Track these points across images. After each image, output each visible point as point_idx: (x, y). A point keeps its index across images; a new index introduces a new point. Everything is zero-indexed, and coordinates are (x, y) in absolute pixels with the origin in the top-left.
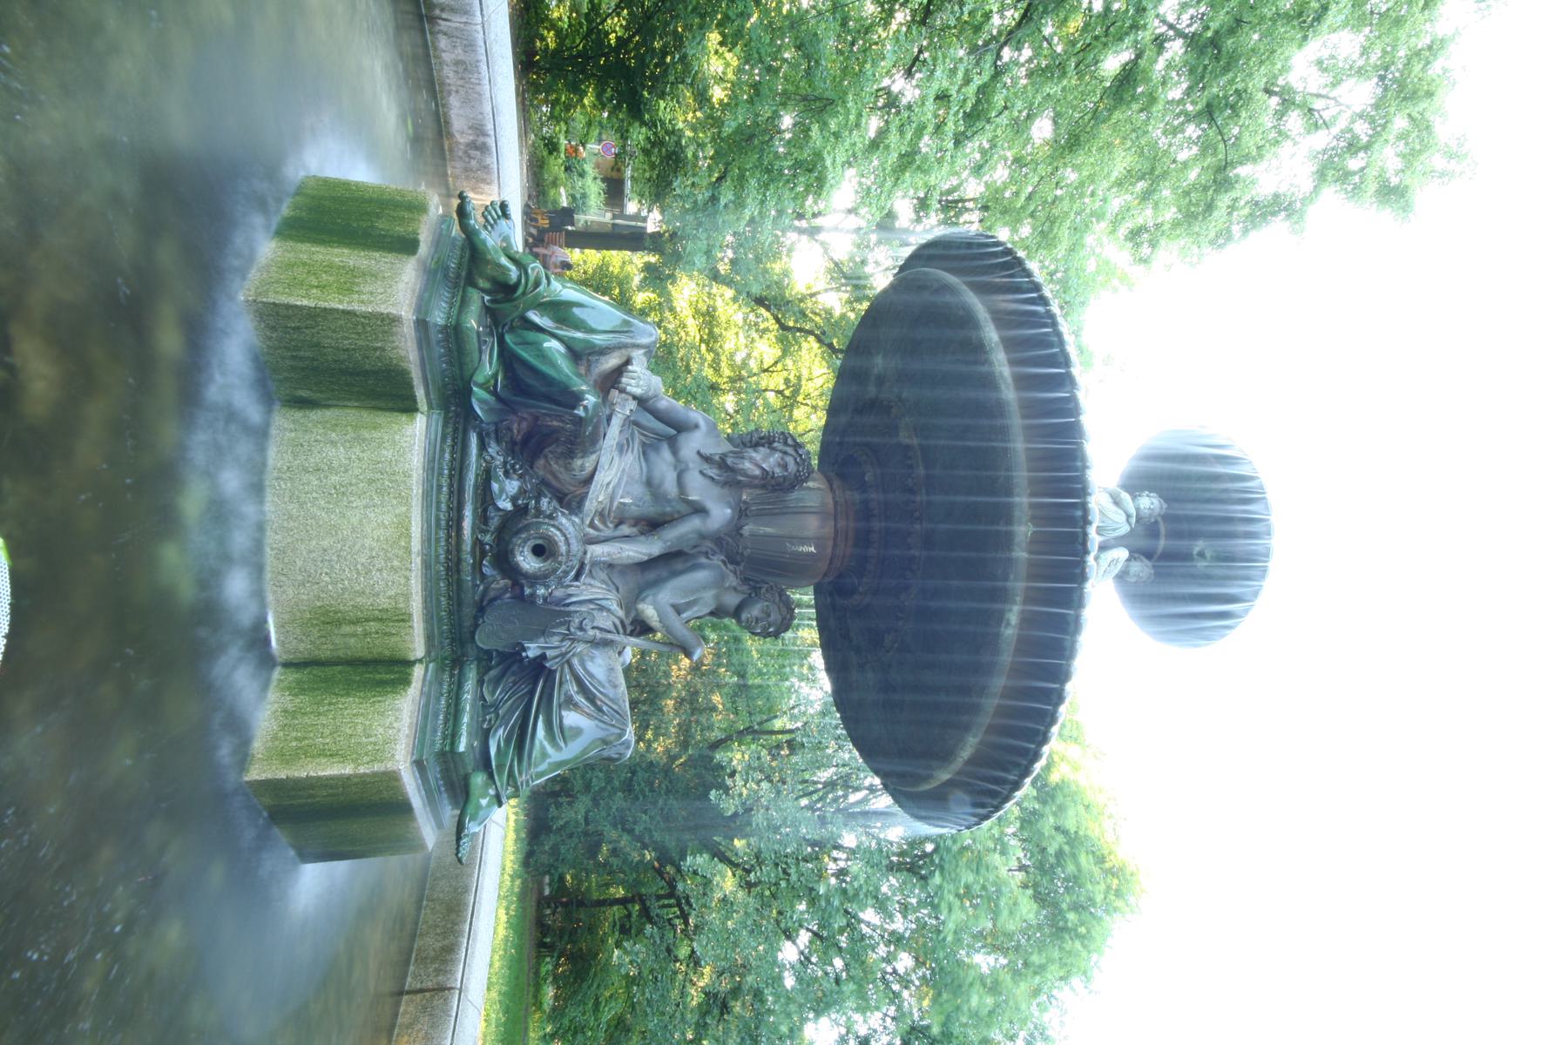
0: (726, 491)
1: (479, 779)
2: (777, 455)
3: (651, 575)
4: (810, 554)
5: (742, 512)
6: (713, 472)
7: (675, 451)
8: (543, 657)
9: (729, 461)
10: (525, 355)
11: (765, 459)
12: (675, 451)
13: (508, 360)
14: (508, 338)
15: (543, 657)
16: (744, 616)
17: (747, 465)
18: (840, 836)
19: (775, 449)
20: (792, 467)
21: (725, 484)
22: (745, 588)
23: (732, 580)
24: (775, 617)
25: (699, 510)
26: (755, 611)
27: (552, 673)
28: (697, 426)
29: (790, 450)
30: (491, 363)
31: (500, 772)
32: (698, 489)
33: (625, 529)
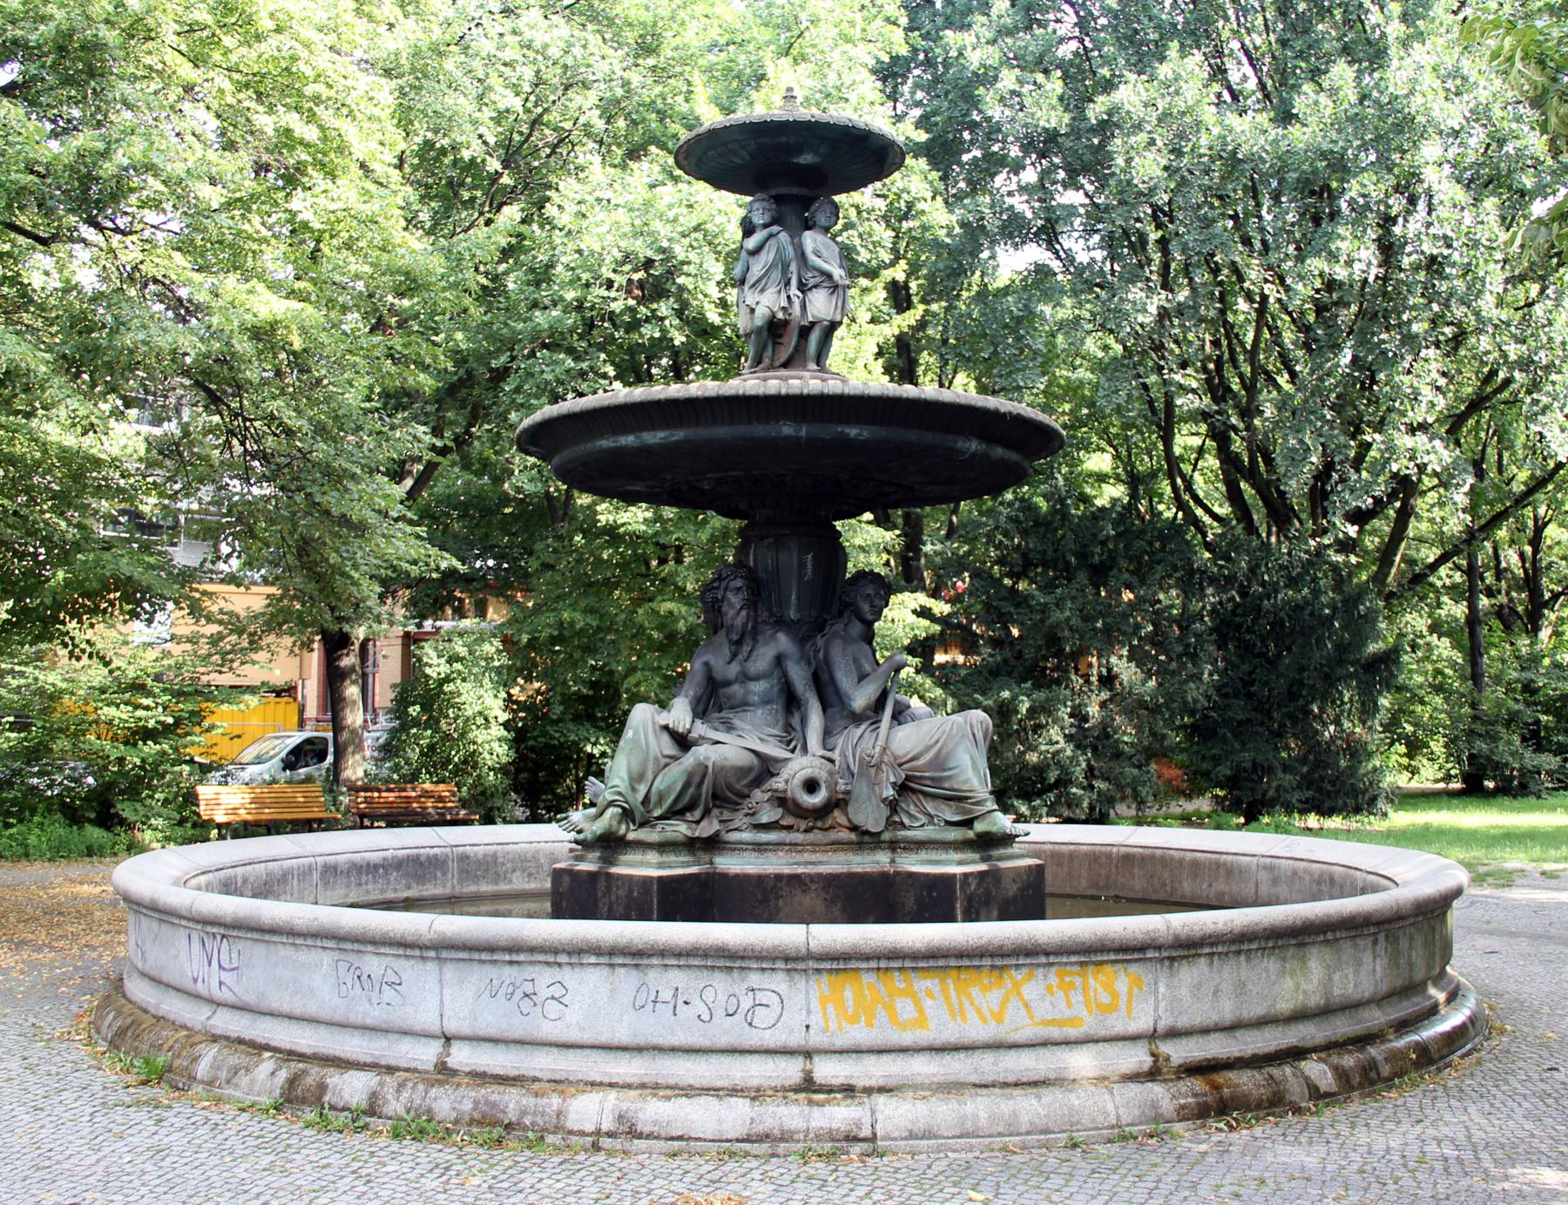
0: (760, 638)
1: (979, 827)
2: (730, 595)
3: (833, 699)
4: (814, 558)
5: (781, 623)
6: (746, 648)
7: (728, 683)
8: (894, 784)
9: (735, 638)
10: (669, 801)
11: (731, 605)
12: (728, 683)
13: (675, 813)
14: (657, 813)
15: (894, 784)
16: (870, 617)
17: (739, 622)
18: (503, 770)
19: (724, 597)
20: (738, 583)
21: (755, 640)
22: (846, 614)
23: (839, 627)
24: (870, 590)
25: (779, 660)
26: (866, 607)
27: (908, 778)
28: (706, 664)
29: (724, 584)
30: (821, 863)
31: (971, 811)
32: (762, 659)
33: (795, 722)
